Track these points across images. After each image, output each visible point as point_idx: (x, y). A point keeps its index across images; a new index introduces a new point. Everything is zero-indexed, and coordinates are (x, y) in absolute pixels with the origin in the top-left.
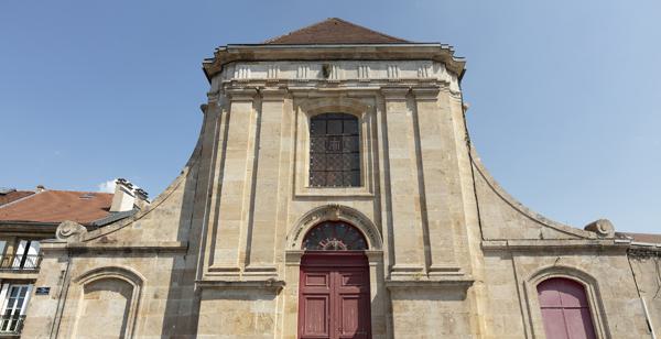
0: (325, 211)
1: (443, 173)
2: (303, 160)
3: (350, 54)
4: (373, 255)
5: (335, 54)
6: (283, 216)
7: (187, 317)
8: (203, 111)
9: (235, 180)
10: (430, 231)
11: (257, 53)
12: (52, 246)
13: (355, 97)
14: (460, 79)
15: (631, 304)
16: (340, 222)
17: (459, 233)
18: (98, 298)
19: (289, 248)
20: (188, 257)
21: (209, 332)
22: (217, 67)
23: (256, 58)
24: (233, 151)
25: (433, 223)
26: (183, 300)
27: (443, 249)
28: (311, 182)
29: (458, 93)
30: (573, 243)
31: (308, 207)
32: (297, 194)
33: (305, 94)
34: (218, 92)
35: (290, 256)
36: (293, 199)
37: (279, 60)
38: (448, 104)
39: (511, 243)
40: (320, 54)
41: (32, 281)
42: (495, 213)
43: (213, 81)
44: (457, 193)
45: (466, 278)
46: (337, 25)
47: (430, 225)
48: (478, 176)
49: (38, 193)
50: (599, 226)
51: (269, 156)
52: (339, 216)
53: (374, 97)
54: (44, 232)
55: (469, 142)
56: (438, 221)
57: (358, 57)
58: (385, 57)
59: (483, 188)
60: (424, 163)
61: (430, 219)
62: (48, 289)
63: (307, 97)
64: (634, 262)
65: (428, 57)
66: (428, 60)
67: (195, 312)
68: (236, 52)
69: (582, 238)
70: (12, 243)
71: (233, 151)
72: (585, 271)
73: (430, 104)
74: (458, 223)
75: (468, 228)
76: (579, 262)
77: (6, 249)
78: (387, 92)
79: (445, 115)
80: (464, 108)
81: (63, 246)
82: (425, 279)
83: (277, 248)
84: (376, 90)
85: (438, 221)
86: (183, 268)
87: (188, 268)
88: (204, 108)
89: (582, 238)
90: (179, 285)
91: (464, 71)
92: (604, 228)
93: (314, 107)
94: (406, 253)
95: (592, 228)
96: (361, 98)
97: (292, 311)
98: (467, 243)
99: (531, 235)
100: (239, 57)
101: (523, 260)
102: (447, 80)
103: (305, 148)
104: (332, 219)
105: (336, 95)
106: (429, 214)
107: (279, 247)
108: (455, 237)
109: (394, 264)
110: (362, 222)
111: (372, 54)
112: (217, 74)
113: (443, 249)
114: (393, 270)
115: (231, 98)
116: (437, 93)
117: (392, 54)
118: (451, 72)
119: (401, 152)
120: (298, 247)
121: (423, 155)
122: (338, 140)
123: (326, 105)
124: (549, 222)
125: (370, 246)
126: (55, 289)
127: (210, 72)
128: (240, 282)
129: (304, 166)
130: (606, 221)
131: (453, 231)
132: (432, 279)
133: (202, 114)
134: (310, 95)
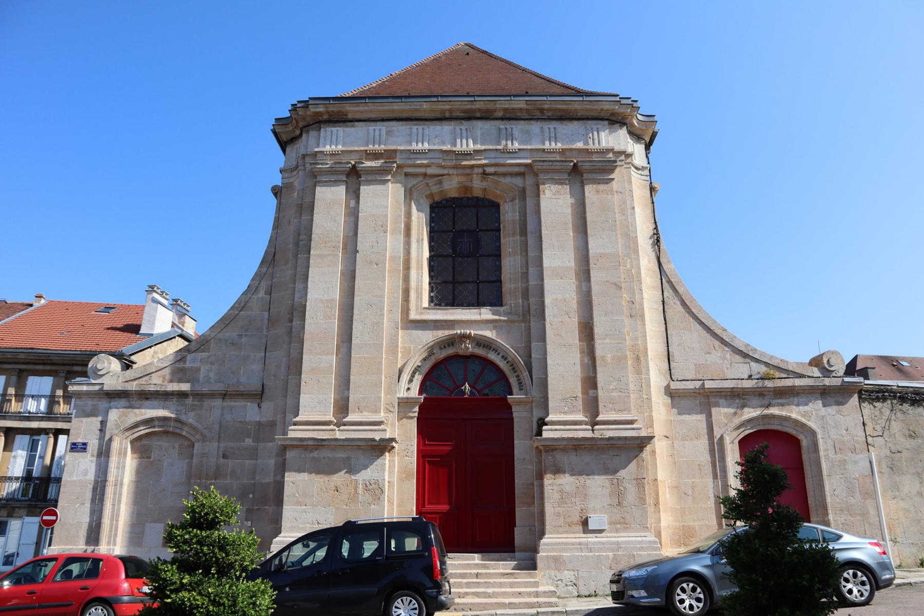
0: (450, 342)
1: (620, 288)
2: (420, 267)
3: (488, 111)
4: (520, 402)
5: (465, 111)
6: (393, 348)
7: (269, 483)
8: (276, 194)
9: (326, 297)
10: (599, 369)
11: (352, 109)
12: (85, 388)
13: (495, 174)
14: (648, 147)
15: (855, 462)
16: (473, 357)
17: (638, 372)
18: (149, 458)
19: (402, 394)
20: (264, 405)
21: (299, 503)
22: (291, 131)
23: (350, 116)
24: (322, 257)
25: (603, 358)
26: (259, 461)
27: (615, 394)
28: (431, 300)
29: (643, 168)
30: (789, 383)
31: (429, 337)
32: (413, 316)
33: (423, 170)
34: (297, 167)
35: (404, 403)
36: (405, 328)
37: (383, 120)
38: (631, 184)
39: (708, 385)
40: (443, 112)
41: (66, 432)
42: (689, 338)
43: (288, 150)
44: (637, 315)
45: (643, 433)
46: (473, 55)
47: (598, 362)
48: (668, 293)
49: (36, 305)
50: (825, 361)
51: (371, 262)
52: (469, 347)
53: (522, 174)
54: (69, 366)
55: (658, 241)
56: (609, 356)
57: (500, 114)
58: (539, 114)
59: (675, 308)
60: (593, 274)
61: (599, 352)
62: (85, 444)
63: (425, 175)
64: (867, 407)
65: (603, 115)
66: (602, 119)
67: (278, 478)
68: (321, 109)
69: (801, 376)
70: (14, 378)
71: (322, 257)
72: (804, 420)
73: (602, 187)
74: (638, 359)
75: (651, 365)
76: (795, 412)
77: (5, 389)
78: (534, 173)
79: (625, 202)
80: (652, 189)
81: (97, 388)
82: (589, 434)
83: (387, 393)
84: (526, 165)
85: (609, 356)
86: (258, 419)
87: (264, 419)
88: (276, 191)
89: (801, 376)
90: (253, 442)
91: (654, 135)
92: (832, 362)
93: (435, 189)
94: (565, 400)
95: (816, 362)
96: (504, 175)
97: (408, 478)
98: (649, 386)
99: (738, 374)
100: (325, 117)
101: (722, 413)
102: (629, 150)
103: (422, 251)
104: (461, 353)
105: (468, 171)
106: (597, 346)
107: (390, 391)
108: (632, 378)
109: (597, 416)
110: (504, 358)
111: (521, 110)
112: (294, 140)
113: (615, 394)
114: (597, 424)
115: (315, 178)
116: (612, 171)
117: (550, 110)
118: (636, 136)
119: (557, 257)
120: (414, 392)
121: (591, 261)
122: (472, 244)
123: (451, 186)
124: (763, 354)
125: (515, 389)
126: (93, 446)
127: (284, 138)
128: (336, 440)
129: (421, 278)
130: (834, 352)
131: (630, 368)
132: (597, 435)
133: (273, 201)
134: (430, 171)
